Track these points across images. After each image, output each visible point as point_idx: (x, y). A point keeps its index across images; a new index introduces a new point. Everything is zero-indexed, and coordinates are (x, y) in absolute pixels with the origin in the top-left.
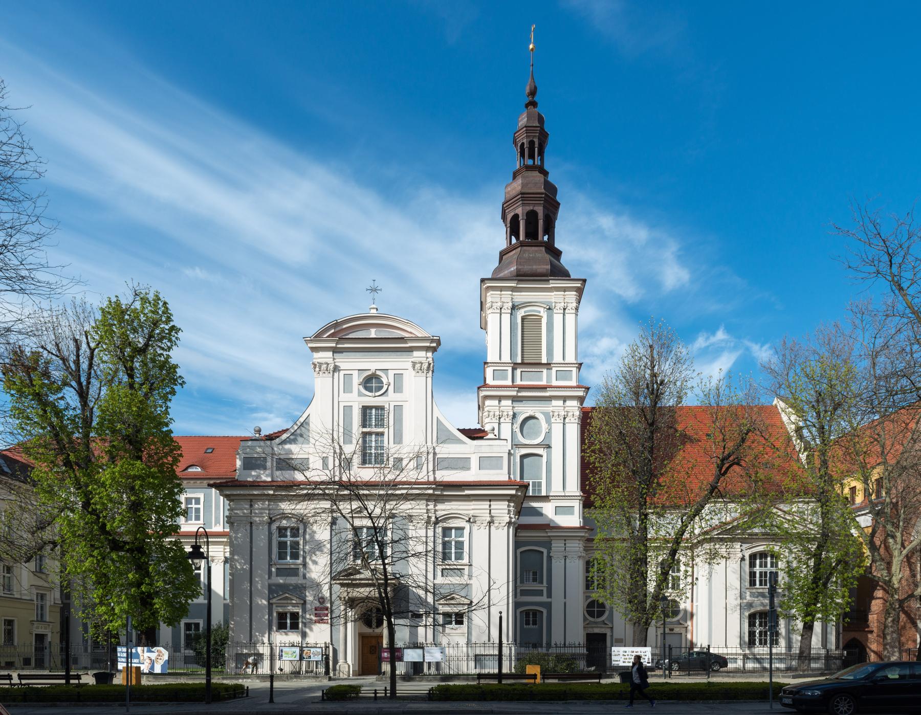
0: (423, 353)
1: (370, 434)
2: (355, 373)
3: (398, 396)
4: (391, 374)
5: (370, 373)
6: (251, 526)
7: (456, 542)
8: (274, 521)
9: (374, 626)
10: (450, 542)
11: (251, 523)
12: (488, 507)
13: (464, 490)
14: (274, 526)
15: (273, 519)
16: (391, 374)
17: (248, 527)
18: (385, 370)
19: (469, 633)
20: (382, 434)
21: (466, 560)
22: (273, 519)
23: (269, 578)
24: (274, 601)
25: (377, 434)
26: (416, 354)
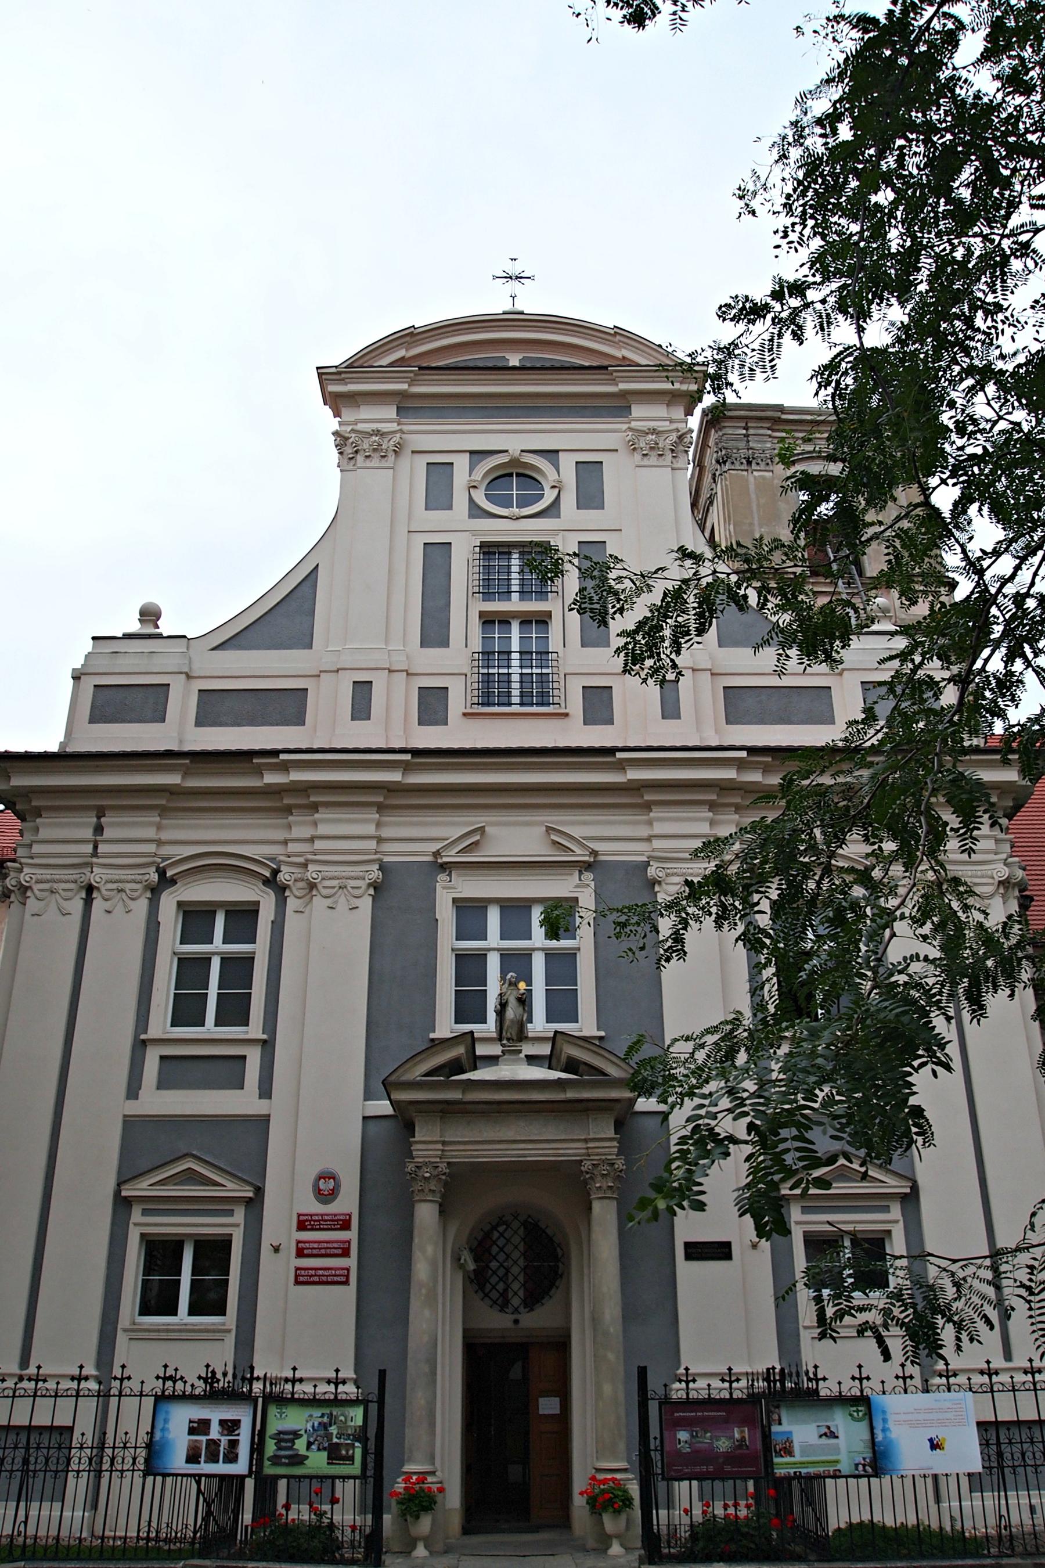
0: (660, 411)
1: (504, 620)
2: (461, 464)
3: (591, 517)
4: (568, 463)
5: (503, 459)
6: (88, 902)
7: (551, 956)
8: (173, 882)
9: (516, 1302)
10: (481, 957)
11: (90, 889)
12: (88, 833)
13: (259, 772)
14: (168, 902)
15: (169, 874)
16: (568, 463)
17: (77, 905)
18: (552, 454)
19: (245, 1342)
20: (543, 620)
21: (255, 1029)
22: (169, 874)
23: (133, 1091)
24: (142, 1188)
25: (527, 620)
26: (637, 411)
